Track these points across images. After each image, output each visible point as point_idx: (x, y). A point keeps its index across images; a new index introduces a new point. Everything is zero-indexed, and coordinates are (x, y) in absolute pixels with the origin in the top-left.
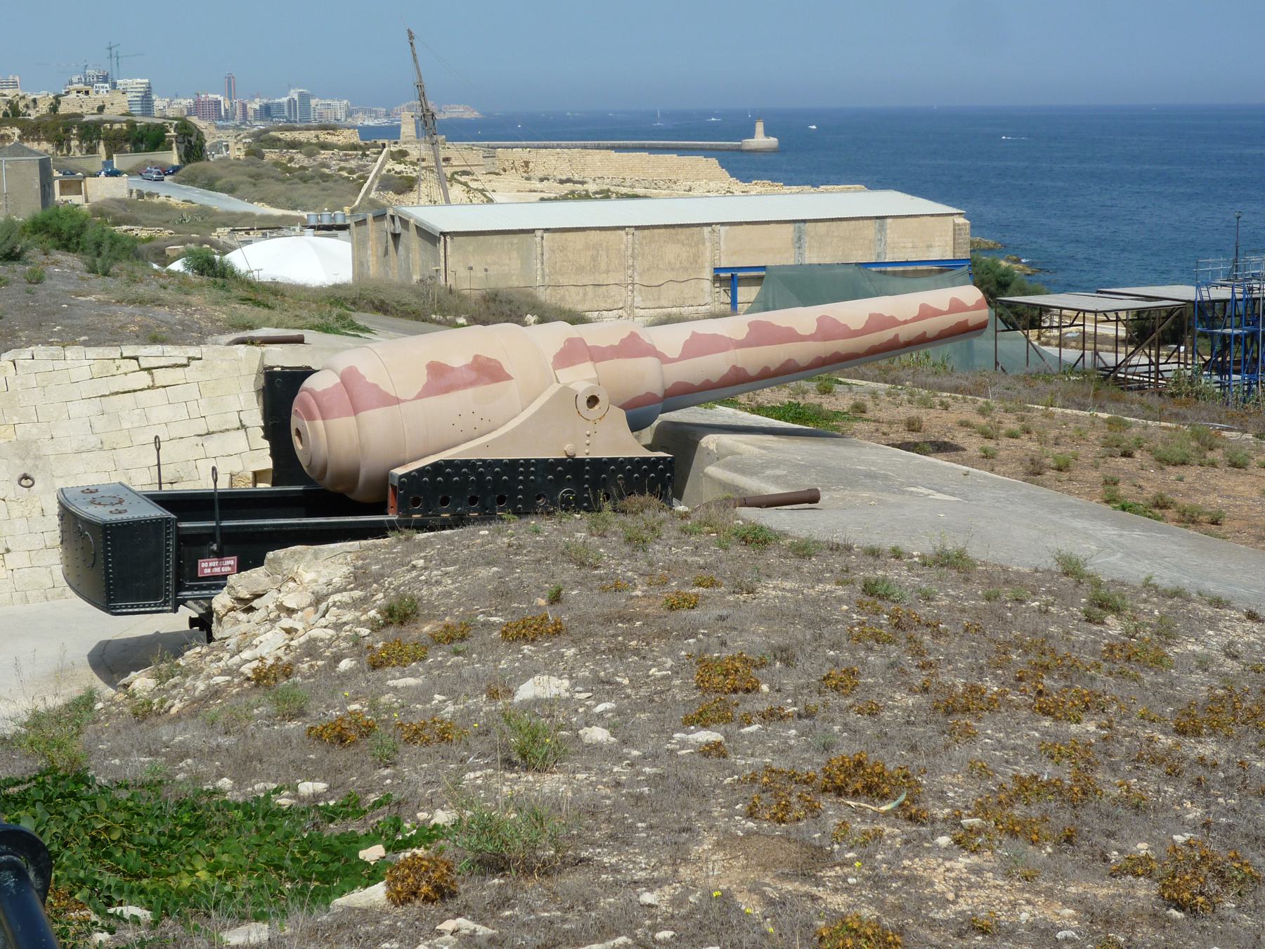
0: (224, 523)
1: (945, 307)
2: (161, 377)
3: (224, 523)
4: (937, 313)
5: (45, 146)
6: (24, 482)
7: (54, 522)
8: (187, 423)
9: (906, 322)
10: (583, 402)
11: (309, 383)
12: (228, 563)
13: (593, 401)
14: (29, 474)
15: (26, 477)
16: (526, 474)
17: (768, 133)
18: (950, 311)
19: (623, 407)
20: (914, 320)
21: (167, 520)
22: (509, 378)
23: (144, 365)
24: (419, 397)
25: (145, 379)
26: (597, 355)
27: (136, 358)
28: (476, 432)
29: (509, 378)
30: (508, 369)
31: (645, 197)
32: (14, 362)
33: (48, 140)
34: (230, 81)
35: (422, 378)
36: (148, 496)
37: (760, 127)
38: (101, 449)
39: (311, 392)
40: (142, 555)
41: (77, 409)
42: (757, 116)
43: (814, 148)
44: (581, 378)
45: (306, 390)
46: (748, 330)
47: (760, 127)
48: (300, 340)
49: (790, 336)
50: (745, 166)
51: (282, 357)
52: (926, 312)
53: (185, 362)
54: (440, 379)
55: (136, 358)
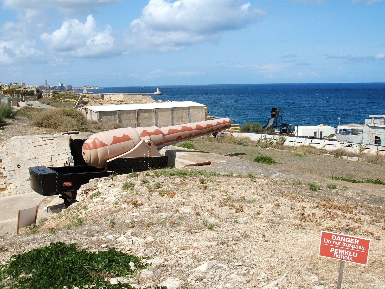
0: (69, 174)
1: (222, 122)
2: (48, 142)
3: (66, 174)
4: (221, 124)
5: (9, 95)
6: (18, 166)
7: (28, 175)
8: (56, 153)
9: (215, 126)
10: (148, 145)
11: (86, 142)
12: (70, 183)
13: (150, 144)
14: (20, 165)
15: (18, 165)
16: (136, 161)
17: (159, 91)
18: (224, 123)
19: (157, 145)
20: (216, 125)
21: (55, 173)
22: (131, 139)
23: (44, 139)
24: (112, 144)
25: (44, 142)
26: (149, 134)
27: (42, 138)
28: (124, 152)
29: (131, 139)
30: (131, 138)
31: (170, 93)
32: (15, 139)
33: (9, 94)
34: (46, 81)
35: (112, 140)
36: (274, 162)
37: (158, 89)
38: (35, 158)
39: (87, 144)
40: (48, 182)
41: (29, 149)
42: (158, 87)
43: (170, 93)
44: (147, 139)
45: (86, 143)
46: (122, 136)
47: (158, 89)
48: (78, 133)
49: (191, 129)
50: (156, 98)
51: (74, 137)
52: (219, 123)
53: (53, 138)
54: (116, 140)
55: (42, 138)
